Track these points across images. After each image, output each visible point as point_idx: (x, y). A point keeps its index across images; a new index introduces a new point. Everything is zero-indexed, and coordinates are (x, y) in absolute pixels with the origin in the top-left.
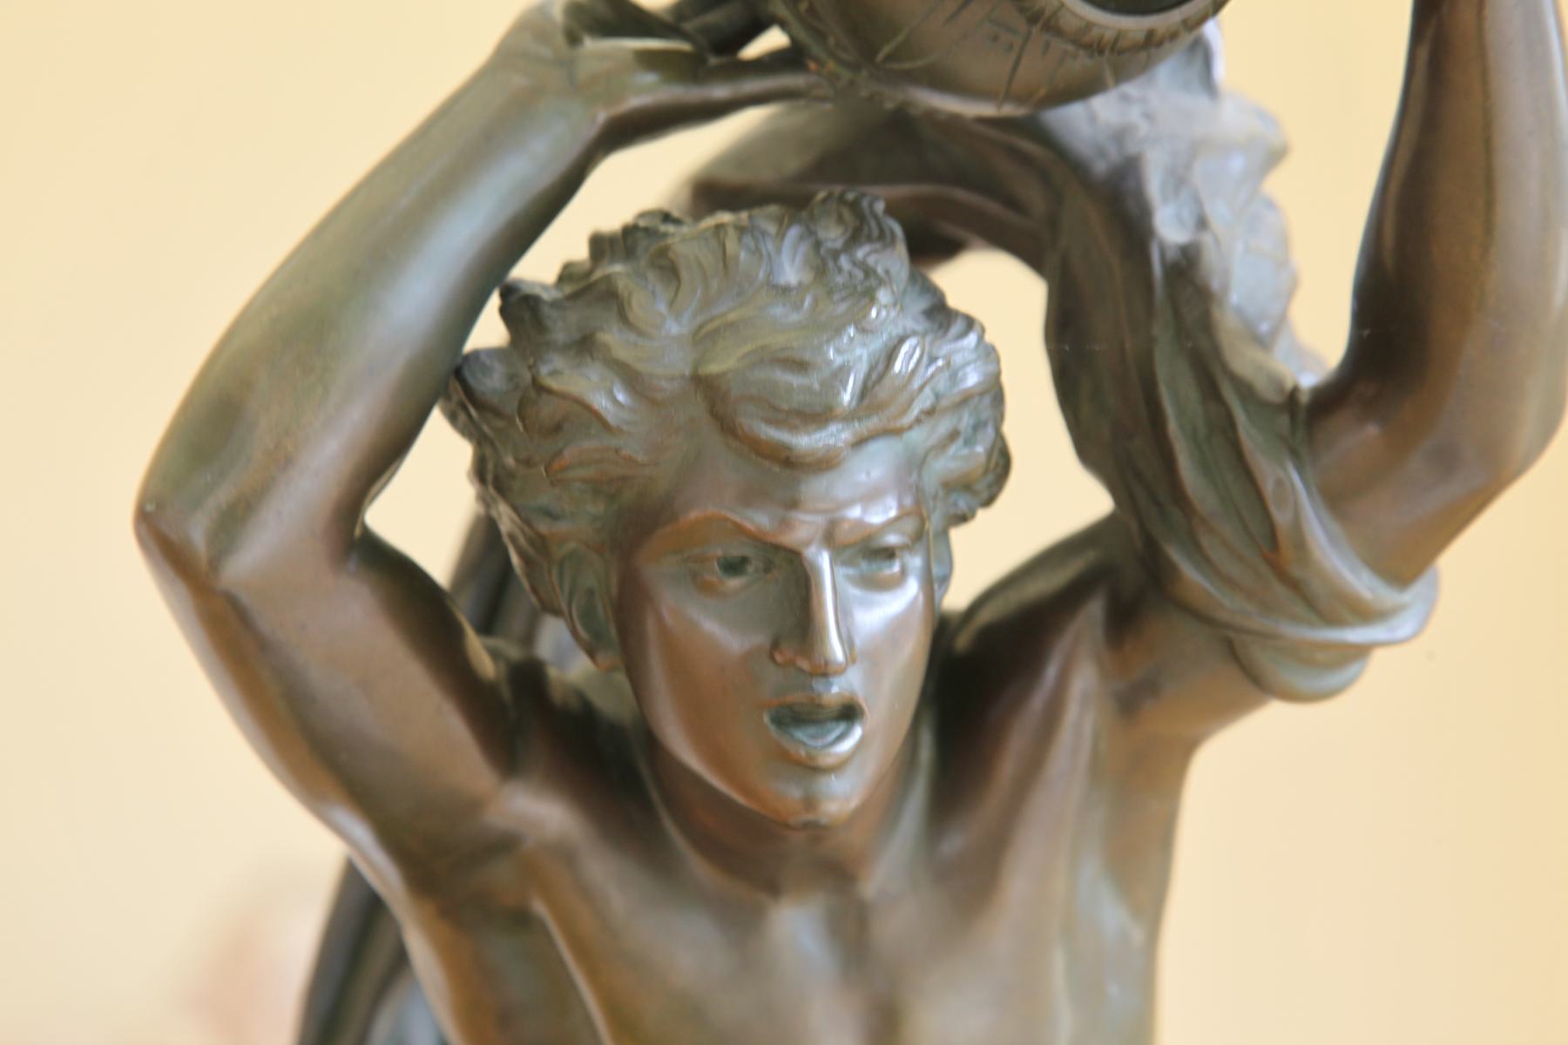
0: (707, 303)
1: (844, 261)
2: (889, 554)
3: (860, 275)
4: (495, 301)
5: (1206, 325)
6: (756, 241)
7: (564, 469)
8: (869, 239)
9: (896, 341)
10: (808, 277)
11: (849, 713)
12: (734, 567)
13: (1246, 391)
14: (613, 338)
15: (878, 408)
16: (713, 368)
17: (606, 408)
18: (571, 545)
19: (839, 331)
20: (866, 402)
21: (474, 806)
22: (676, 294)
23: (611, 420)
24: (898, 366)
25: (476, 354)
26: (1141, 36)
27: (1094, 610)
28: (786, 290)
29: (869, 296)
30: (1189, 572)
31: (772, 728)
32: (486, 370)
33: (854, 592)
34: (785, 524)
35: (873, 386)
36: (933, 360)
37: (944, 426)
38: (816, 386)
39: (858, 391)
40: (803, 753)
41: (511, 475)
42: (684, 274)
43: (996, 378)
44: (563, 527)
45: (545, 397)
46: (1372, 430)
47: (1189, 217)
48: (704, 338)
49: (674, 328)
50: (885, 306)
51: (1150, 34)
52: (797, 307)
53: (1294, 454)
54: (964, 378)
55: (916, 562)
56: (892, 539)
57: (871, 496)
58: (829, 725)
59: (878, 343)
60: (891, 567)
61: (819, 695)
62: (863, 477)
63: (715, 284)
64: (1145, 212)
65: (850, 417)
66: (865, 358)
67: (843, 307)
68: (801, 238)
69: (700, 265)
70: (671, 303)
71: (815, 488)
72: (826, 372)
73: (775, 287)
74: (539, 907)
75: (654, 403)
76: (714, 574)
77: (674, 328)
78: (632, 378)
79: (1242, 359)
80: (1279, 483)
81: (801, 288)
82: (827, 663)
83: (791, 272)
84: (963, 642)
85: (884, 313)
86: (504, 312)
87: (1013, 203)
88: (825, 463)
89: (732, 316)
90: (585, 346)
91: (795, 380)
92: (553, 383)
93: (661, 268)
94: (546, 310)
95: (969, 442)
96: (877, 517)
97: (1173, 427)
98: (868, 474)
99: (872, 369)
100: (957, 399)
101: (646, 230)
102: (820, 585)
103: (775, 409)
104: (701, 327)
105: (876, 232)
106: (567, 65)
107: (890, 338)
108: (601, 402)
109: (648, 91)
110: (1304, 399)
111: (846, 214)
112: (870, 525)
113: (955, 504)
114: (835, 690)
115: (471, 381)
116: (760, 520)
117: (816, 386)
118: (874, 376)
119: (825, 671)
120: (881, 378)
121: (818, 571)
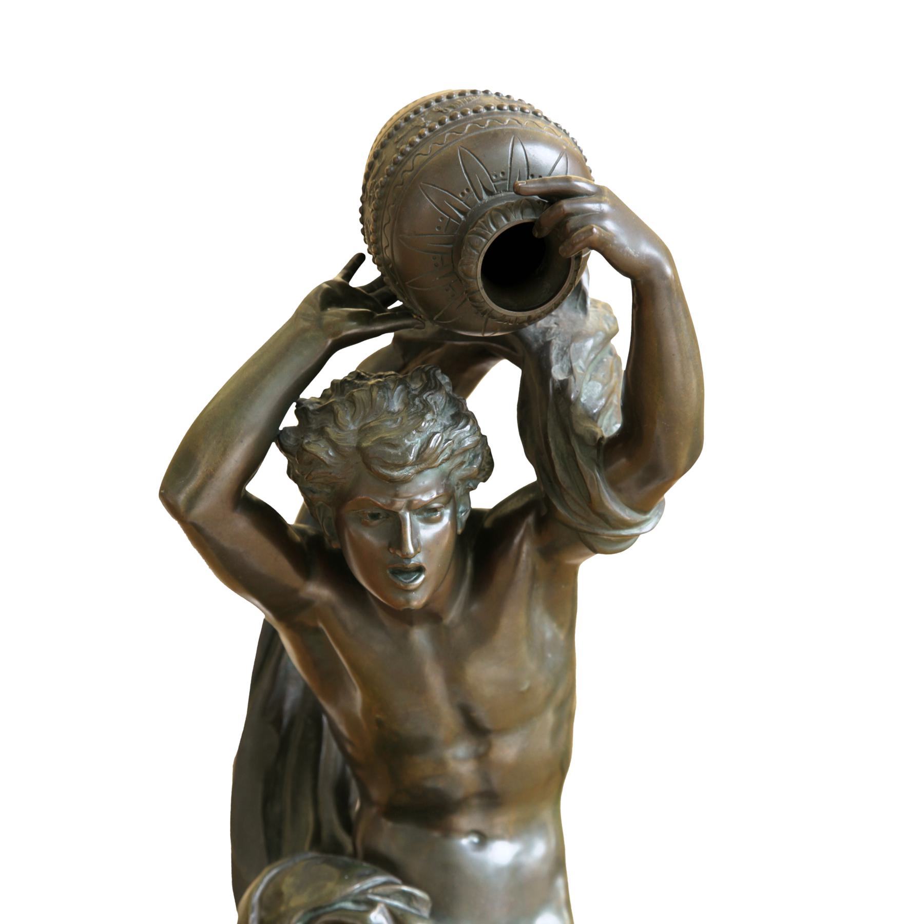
0: (364, 418)
1: (417, 401)
2: (435, 510)
3: (421, 406)
4: (293, 407)
5: (569, 414)
7: (314, 478)
8: (430, 389)
10: (401, 407)
11: (420, 569)
12: (375, 516)
13: (581, 439)
14: (331, 430)
16: (364, 445)
17: (326, 458)
18: (320, 503)
19: (409, 433)
20: (419, 459)
21: (295, 591)
22: (355, 410)
23: (327, 462)
24: (432, 444)
26: (526, 319)
27: (530, 519)
28: (393, 413)
29: (422, 417)
30: (560, 509)
31: (391, 576)
32: (288, 437)
33: (420, 524)
34: (393, 503)
35: (422, 453)
36: (447, 440)
37: (458, 460)
38: (400, 454)
39: (416, 455)
40: (402, 585)
41: (298, 476)
42: (358, 405)
43: (484, 439)
44: (316, 496)
45: (305, 452)
46: (623, 461)
47: (567, 370)
48: (363, 431)
49: (352, 427)
50: (428, 421)
51: (529, 317)
52: (395, 422)
53: (598, 466)
54: (464, 444)
55: (447, 512)
56: (435, 505)
57: (426, 490)
58: (412, 574)
59: (424, 436)
60: (436, 515)
61: (407, 565)
62: (421, 484)
63: (368, 410)
64: (549, 367)
65: (413, 464)
66: (419, 441)
67: (412, 422)
68: (402, 390)
70: (352, 417)
71: (404, 489)
72: (404, 448)
73: (389, 412)
74: (321, 625)
75: (343, 456)
76: (368, 520)
77: (352, 427)
78: (335, 446)
79: (583, 426)
80: (592, 477)
81: (399, 412)
82: (407, 554)
83: (396, 405)
85: (427, 424)
86: (297, 413)
88: (405, 481)
89: (372, 424)
90: (321, 432)
91: (392, 451)
92: (307, 447)
93: (350, 402)
94: (310, 415)
95: (471, 464)
96: (426, 498)
97: (553, 454)
98: (424, 483)
99: (422, 446)
100: (461, 451)
101: (349, 382)
102: (405, 525)
103: (385, 462)
104: (362, 427)
105: (433, 385)
106: (319, 319)
107: (430, 433)
108: (323, 456)
110: (604, 443)
111: (424, 376)
112: (424, 501)
113: (468, 485)
114: (412, 562)
115: (282, 441)
116: (382, 501)
117: (400, 454)
118: (422, 449)
119: (408, 557)
120: (425, 450)
121: (405, 520)
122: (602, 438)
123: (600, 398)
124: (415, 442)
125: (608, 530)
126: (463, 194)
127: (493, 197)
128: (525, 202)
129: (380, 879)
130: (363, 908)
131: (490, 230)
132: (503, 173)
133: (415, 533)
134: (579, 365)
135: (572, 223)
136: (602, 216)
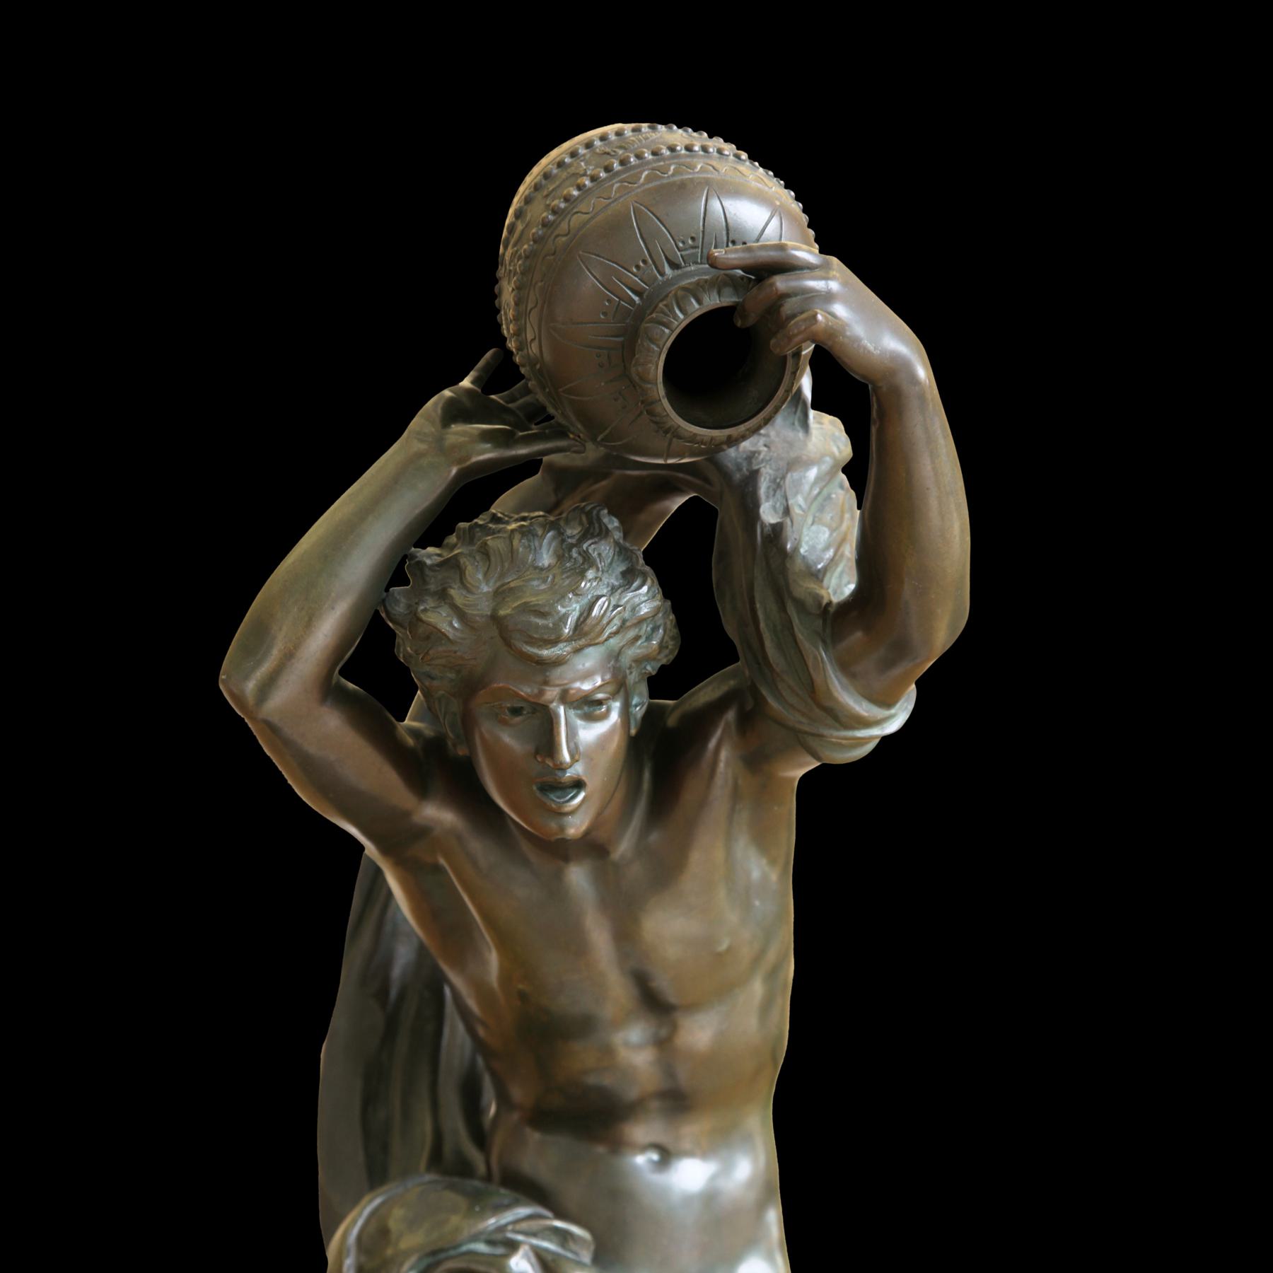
0: (502, 576)
1: (574, 553)
2: (600, 703)
5: (784, 570)
6: (529, 541)
7: (432, 659)
8: (593, 536)
10: (553, 561)
11: (578, 785)
12: (516, 711)
14: (455, 593)
16: (502, 612)
18: (441, 692)
19: (563, 597)
20: (577, 632)
21: (407, 814)
22: (489, 565)
23: (451, 636)
24: (595, 612)
26: (724, 439)
27: (731, 715)
28: (542, 569)
29: (582, 575)
30: (771, 701)
31: (538, 794)
33: (579, 722)
34: (541, 693)
35: (581, 624)
37: (631, 634)
38: (551, 625)
39: (573, 627)
40: (553, 806)
42: (493, 559)
44: (436, 683)
45: (420, 623)
46: (859, 635)
47: (781, 510)
48: (500, 594)
49: (485, 589)
51: (729, 437)
52: (545, 581)
53: (824, 642)
54: (639, 611)
55: (616, 705)
56: (600, 696)
57: (587, 676)
58: (568, 790)
59: (585, 601)
60: (600, 709)
61: (560, 778)
62: (580, 667)
63: (506, 565)
64: (757, 505)
65: (569, 640)
66: (578, 608)
68: (554, 538)
69: (499, 551)
70: (485, 574)
71: (556, 674)
72: (557, 617)
73: (536, 568)
74: (442, 861)
75: (472, 628)
76: (507, 716)
77: (485, 589)
78: (461, 615)
79: (803, 587)
80: (815, 658)
81: (550, 568)
82: (561, 763)
85: (588, 585)
88: (558, 662)
89: (512, 585)
90: (443, 595)
91: (540, 622)
92: (423, 616)
93: (483, 553)
94: (427, 572)
95: (649, 639)
96: (587, 686)
97: (762, 625)
98: (584, 665)
99: (581, 615)
100: (635, 621)
102: (558, 723)
103: (531, 637)
104: (498, 588)
105: (597, 530)
106: (440, 440)
107: (592, 597)
108: (445, 628)
110: (832, 610)
111: (584, 518)
112: (584, 691)
113: (645, 668)
114: (568, 775)
116: (526, 690)
117: (551, 625)
118: (582, 619)
119: (562, 768)
120: (585, 619)
121: (558, 716)
122: (830, 603)
123: (827, 548)
124: (572, 609)
125: (838, 730)
126: (638, 267)
127: (679, 272)
128: (723, 278)
129: (523, 1211)
130: (500, 1251)
131: (675, 317)
132: (693, 239)
133: (572, 734)
134: (798, 502)
135: (788, 307)
136: (829, 297)
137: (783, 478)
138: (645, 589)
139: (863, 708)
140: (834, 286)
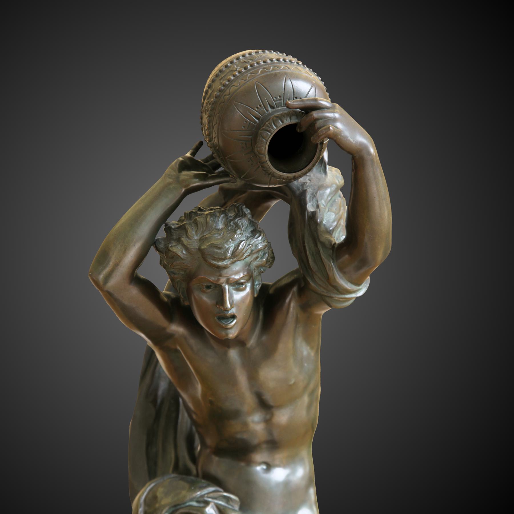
0: (203, 232)
1: (232, 223)
2: (242, 284)
5: (316, 230)
7: (175, 266)
8: (239, 216)
9: (240, 242)
10: (223, 227)
11: (233, 317)
12: (208, 287)
13: (323, 244)
14: (184, 239)
15: (237, 256)
16: (203, 247)
18: (178, 280)
19: (227, 241)
20: (233, 255)
21: (164, 329)
22: (198, 228)
23: (182, 257)
24: (240, 247)
25: (158, 240)
26: (293, 177)
27: (295, 289)
29: (235, 232)
30: (311, 283)
31: (217, 321)
32: (160, 243)
33: (234, 292)
34: (219, 280)
35: (235, 252)
37: (255, 256)
38: (222, 252)
39: (231, 253)
40: (223, 325)
41: (166, 265)
42: (199, 226)
44: (176, 276)
45: (170, 252)
46: (347, 256)
47: (315, 206)
48: (202, 240)
49: (196, 238)
50: (238, 234)
51: (294, 176)
52: (220, 235)
53: (333, 259)
54: (258, 247)
55: (249, 285)
56: (242, 281)
57: (237, 273)
58: (229, 319)
59: (236, 243)
60: (242, 286)
61: (226, 314)
62: (234, 269)
63: (204, 228)
64: (306, 204)
65: (230, 258)
66: (233, 245)
68: (224, 217)
69: (202, 223)
70: (196, 232)
71: (225, 272)
72: (225, 249)
73: (216, 229)
74: (179, 348)
75: (191, 254)
76: (205, 289)
77: (196, 238)
78: (186, 248)
79: (324, 237)
80: (329, 266)
81: (222, 229)
82: (227, 308)
84: (271, 291)
85: (238, 236)
87: (285, 194)
88: (225, 267)
89: (207, 236)
90: (179, 240)
91: (218, 251)
92: (171, 249)
93: (195, 223)
94: (173, 231)
95: (262, 258)
96: (237, 277)
97: (308, 252)
98: (236, 268)
99: (235, 248)
100: (256, 251)
102: (225, 292)
103: (214, 257)
104: (201, 237)
105: (241, 214)
106: (178, 178)
107: (239, 241)
108: (180, 253)
109: (197, 183)
110: (336, 246)
111: (236, 209)
112: (236, 279)
113: (260, 270)
114: (229, 313)
116: (212, 279)
117: (222, 252)
118: (235, 250)
119: (227, 310)
120: (236, 250)
121: (225, 289)
122: (335, 244)
123: (334, 221)
125: (338, 295)
126: (257, 108)
127: (274, 110)
128: (292, 112)
129: (211, 489)
130: (202, 505)
131: (273, 128)
132: (280, 96)
133: (231, 296)
134: (322, 203)
135: (318, 124)
136: (335, 120)
137: (316, 193)
138: (260, 238)
139: (348, 286)
140: (337, 115)
